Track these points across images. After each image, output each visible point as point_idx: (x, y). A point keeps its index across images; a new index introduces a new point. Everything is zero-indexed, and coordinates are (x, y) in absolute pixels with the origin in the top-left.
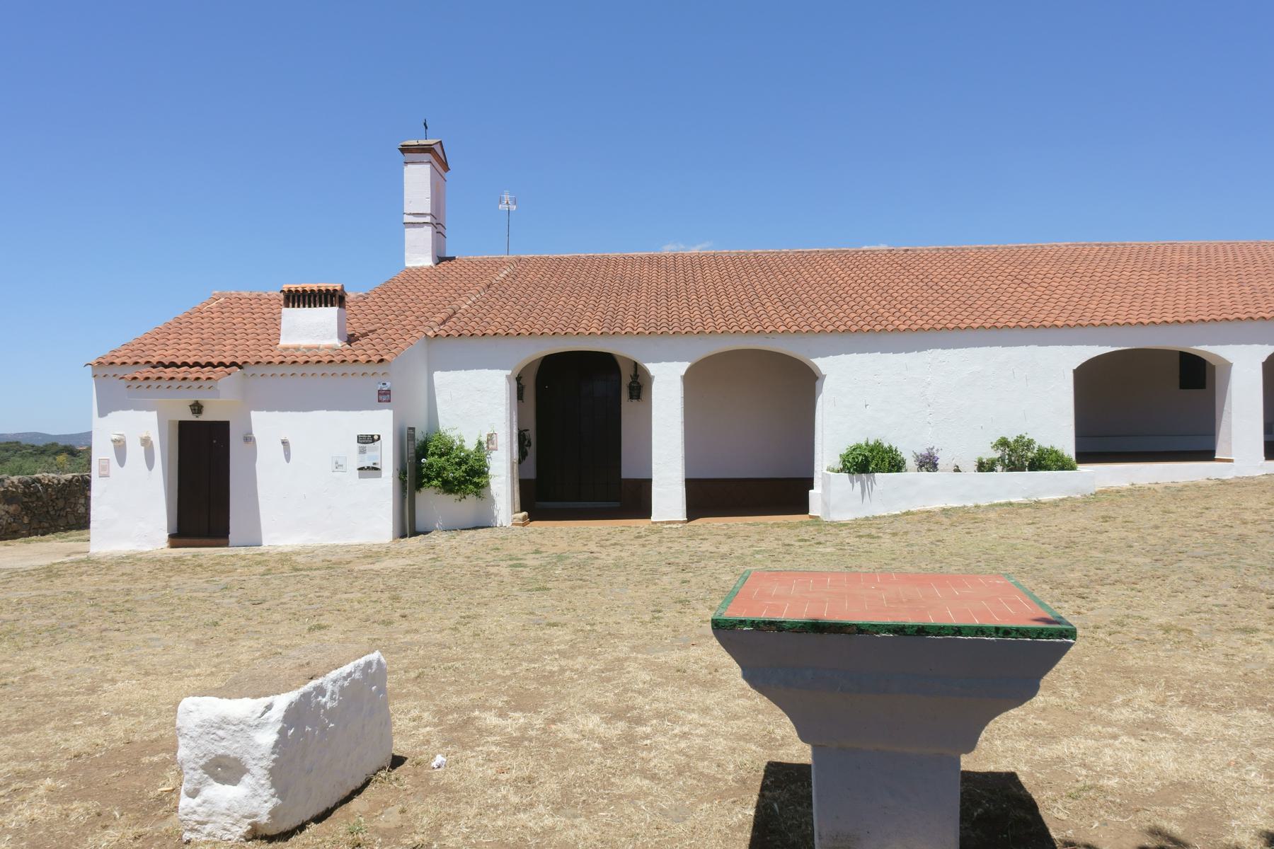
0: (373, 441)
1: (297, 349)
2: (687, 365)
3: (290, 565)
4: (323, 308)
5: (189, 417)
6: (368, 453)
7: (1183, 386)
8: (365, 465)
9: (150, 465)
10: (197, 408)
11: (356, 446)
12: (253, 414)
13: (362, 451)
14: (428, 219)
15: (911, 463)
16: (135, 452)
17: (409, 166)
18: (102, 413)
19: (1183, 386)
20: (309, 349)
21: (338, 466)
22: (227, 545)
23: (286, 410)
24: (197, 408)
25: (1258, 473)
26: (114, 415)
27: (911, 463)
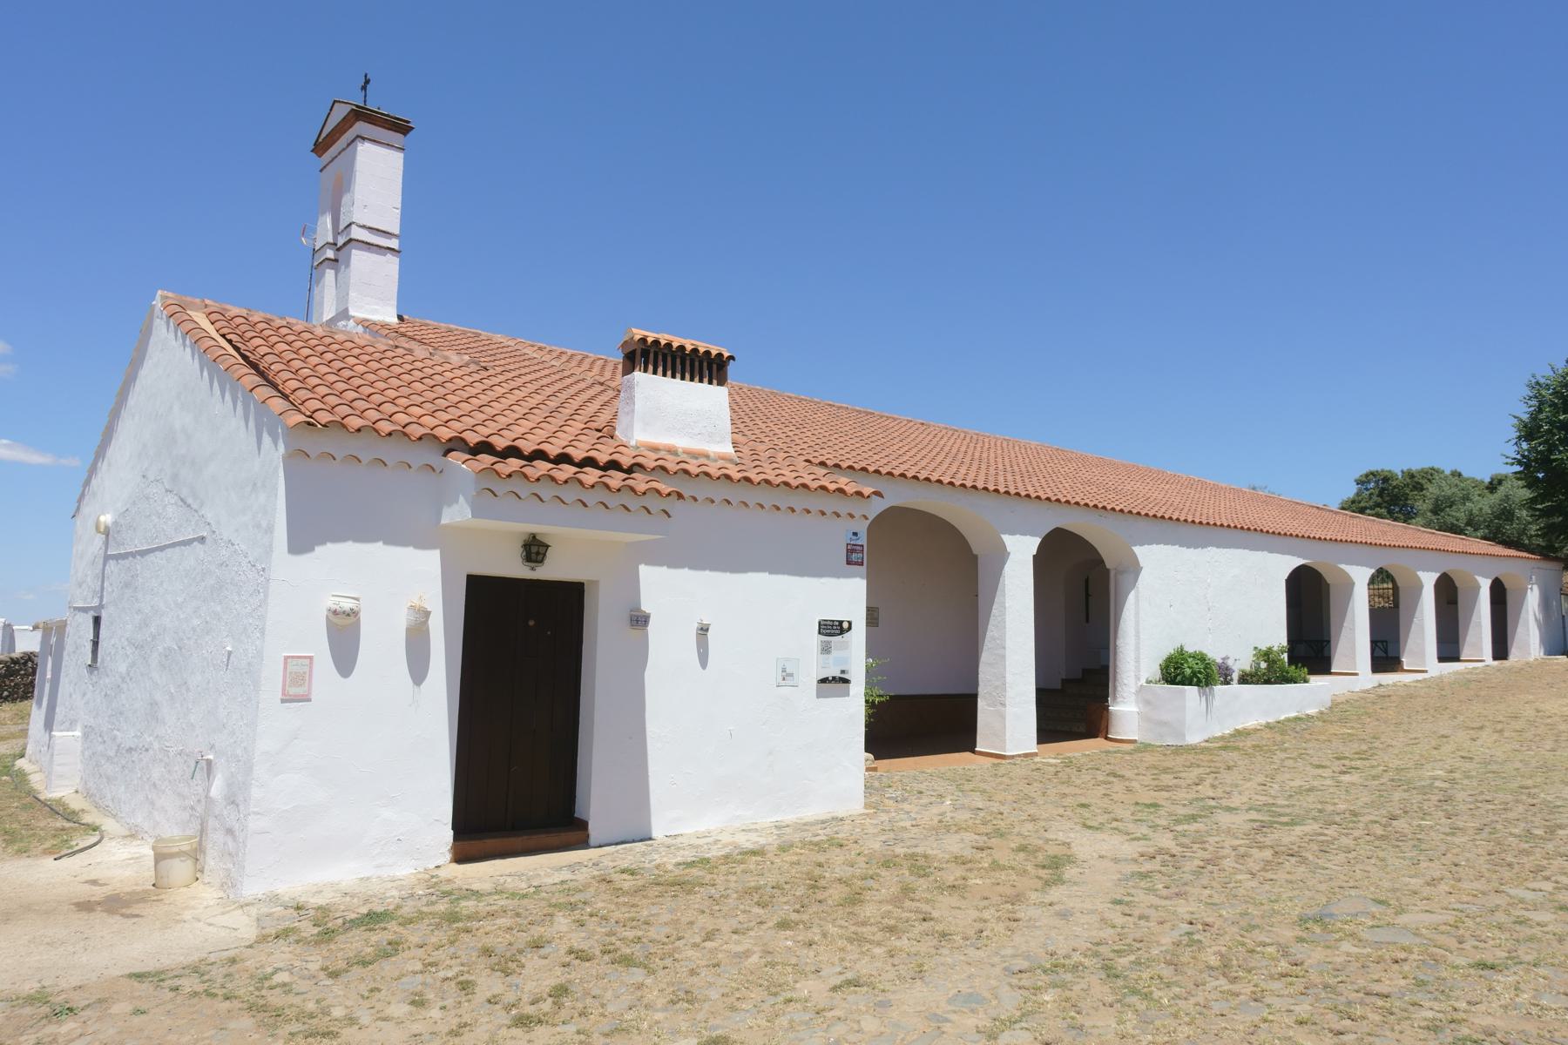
0: (842, 631)
1: (672, 451)
2: (1038, 541)
3: (690, 879)
4: (705, 385)
5: (514, 567)
6: (834, 653)
7: (472, 580)
8: (830, 673)
9: (418, 670)
10: (534, 550)
11: (815, 639)
12: (643, 569)
13: (826, 649)
14: (394, 244)
15: (1235, 676)
16: (382, 642)
17: (367, 145)
18: (300, 543)
19: (472, 580)
20: (695, 455)
21: (786, 675)
22: (584, 843)
23: (703, 568)
24: (534, 550)
25: (1369, 686)
26: (328, 552)
27: (1235, 676)
